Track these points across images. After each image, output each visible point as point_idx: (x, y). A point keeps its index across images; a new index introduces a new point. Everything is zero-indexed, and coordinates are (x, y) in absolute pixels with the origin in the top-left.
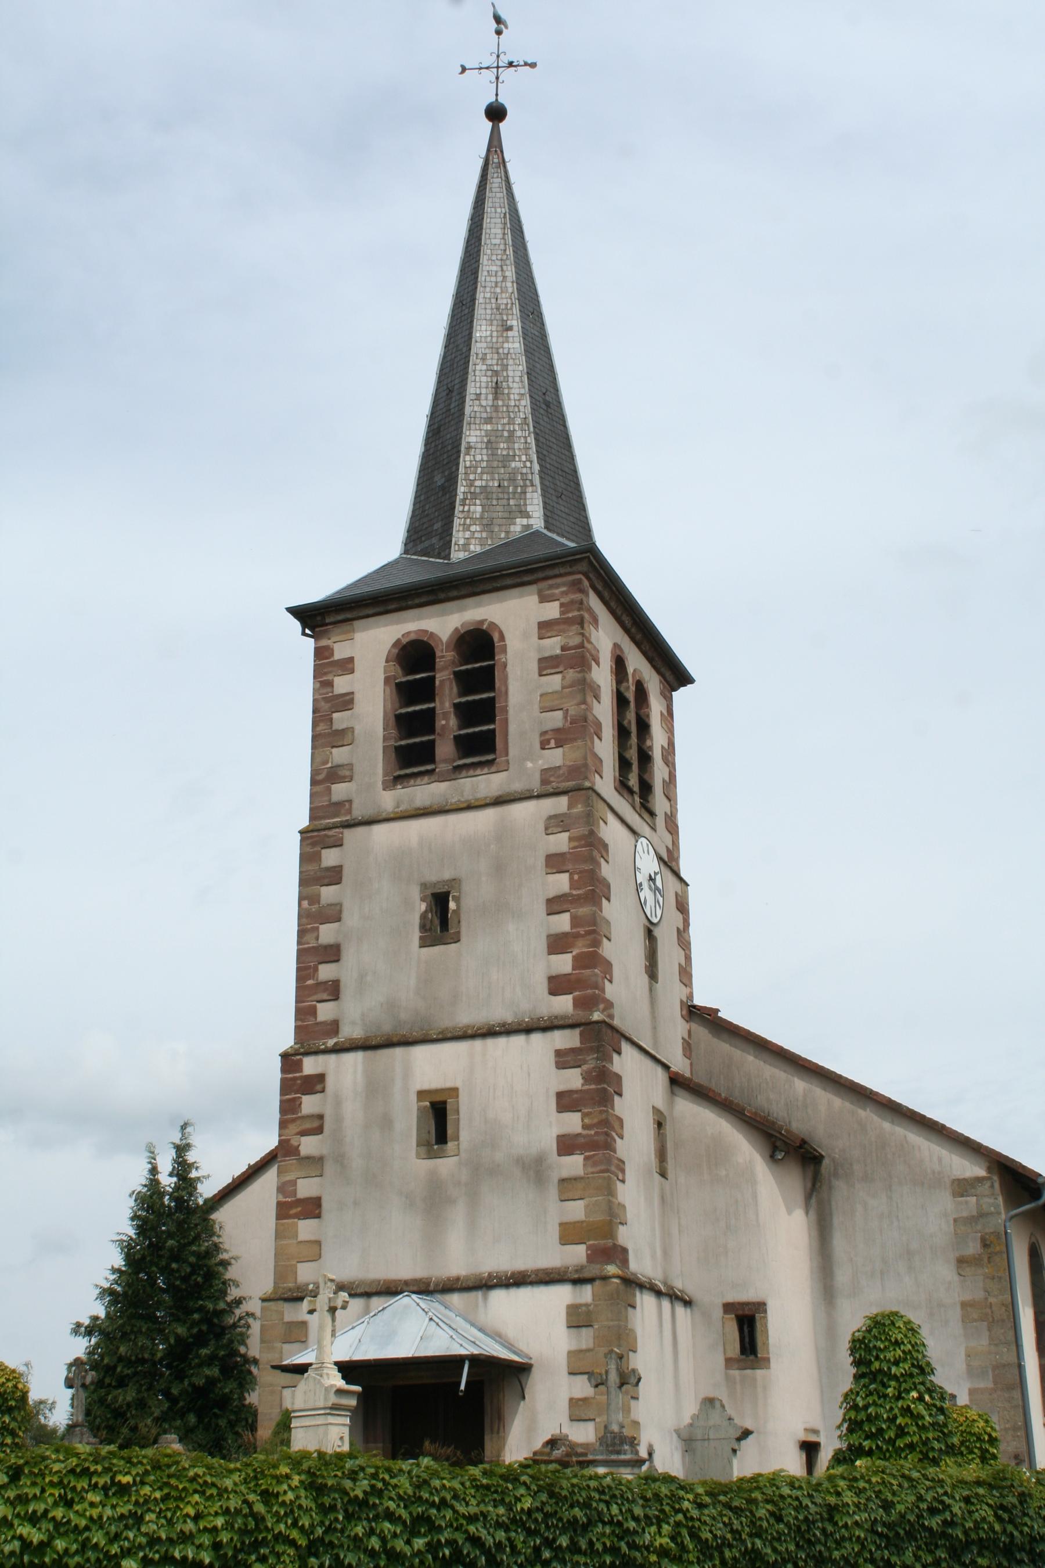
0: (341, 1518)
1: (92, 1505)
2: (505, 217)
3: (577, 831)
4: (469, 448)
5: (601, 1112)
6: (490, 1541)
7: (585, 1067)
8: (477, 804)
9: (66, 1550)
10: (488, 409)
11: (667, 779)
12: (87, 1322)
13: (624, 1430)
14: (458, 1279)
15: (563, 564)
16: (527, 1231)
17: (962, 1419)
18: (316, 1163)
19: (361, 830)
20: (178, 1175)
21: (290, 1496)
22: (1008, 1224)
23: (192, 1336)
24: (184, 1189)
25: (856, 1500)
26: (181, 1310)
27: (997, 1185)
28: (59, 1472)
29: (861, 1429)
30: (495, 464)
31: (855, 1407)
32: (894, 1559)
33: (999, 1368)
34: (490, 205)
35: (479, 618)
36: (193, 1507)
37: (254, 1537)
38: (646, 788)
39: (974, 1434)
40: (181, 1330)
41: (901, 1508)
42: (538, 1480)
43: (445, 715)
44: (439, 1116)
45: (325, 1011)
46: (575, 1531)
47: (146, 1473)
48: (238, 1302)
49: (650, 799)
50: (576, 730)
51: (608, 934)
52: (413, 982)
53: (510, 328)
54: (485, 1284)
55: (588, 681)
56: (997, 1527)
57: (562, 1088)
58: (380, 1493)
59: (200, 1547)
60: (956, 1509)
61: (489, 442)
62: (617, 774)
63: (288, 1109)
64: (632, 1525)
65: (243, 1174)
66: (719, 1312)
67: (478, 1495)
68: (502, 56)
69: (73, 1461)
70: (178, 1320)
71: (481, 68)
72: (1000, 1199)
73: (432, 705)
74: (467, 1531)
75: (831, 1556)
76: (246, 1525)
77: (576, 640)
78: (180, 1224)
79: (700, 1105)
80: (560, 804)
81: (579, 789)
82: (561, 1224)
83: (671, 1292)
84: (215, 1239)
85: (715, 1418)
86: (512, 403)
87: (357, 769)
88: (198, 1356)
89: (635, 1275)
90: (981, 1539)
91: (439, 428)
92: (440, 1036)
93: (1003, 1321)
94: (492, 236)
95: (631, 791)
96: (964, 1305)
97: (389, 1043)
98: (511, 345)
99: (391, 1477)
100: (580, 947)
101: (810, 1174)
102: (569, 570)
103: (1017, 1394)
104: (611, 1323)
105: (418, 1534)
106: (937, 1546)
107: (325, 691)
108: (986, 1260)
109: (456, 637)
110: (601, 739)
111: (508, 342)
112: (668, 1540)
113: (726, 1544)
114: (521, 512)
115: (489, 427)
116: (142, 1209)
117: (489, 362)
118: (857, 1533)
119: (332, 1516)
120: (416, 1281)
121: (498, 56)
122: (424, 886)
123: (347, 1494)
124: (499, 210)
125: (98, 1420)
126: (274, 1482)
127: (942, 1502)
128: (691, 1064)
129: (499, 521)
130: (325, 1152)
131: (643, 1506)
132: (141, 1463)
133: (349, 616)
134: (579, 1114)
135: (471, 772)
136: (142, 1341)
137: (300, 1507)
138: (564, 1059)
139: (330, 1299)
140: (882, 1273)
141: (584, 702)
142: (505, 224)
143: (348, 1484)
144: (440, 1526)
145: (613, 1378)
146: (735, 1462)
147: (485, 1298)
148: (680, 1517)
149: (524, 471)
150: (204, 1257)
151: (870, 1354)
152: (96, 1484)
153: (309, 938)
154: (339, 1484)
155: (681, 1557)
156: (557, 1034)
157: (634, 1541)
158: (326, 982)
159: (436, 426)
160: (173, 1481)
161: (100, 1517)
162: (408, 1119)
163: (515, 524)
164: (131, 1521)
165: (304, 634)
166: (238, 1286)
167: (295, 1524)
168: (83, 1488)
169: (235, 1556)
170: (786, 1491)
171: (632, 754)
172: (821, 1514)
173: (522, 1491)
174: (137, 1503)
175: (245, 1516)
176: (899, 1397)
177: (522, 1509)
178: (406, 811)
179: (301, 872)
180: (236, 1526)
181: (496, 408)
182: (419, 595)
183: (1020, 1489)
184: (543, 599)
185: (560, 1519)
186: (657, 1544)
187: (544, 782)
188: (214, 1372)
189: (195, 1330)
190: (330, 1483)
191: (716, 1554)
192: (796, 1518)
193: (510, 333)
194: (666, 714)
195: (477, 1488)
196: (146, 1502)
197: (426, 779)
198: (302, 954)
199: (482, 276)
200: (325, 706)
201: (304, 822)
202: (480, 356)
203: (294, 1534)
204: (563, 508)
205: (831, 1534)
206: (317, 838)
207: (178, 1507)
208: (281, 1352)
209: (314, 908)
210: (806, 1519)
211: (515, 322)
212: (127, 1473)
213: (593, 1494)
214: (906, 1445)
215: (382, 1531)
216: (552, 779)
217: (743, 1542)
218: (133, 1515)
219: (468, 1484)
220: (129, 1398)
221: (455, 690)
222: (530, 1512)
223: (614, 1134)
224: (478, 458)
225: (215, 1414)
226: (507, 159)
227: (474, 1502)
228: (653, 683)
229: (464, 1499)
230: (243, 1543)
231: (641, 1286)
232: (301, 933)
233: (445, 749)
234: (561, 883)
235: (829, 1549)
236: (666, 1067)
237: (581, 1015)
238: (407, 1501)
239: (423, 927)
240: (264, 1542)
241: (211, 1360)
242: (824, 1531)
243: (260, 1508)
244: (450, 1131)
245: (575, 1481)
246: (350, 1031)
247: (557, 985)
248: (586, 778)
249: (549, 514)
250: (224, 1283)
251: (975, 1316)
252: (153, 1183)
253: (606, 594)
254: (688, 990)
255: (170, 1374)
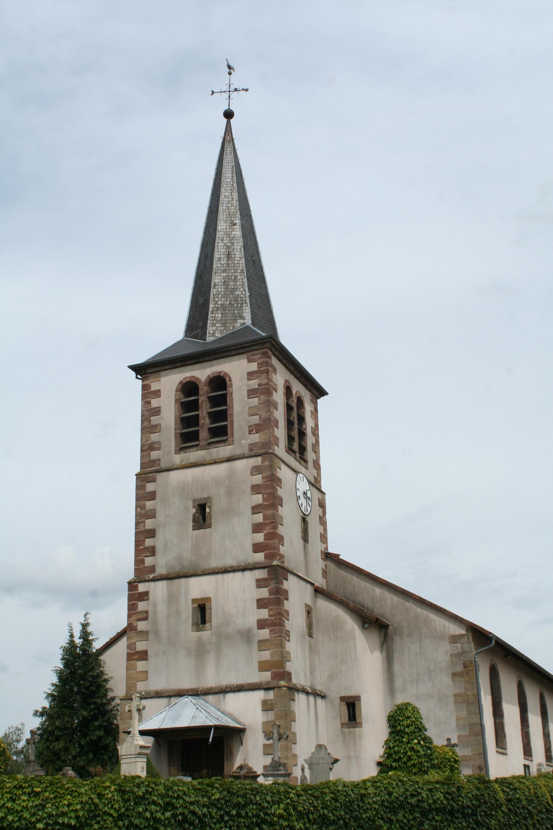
0: (132, 804)
1: (24, 801)
2: (233, 168)
3: (265, 474)
4: (215, 285)
5: (277, 608)
6: (200, 813)
7: (270, 587)
8: (219, 461)
9: (13, 820)
10: (225, 265)
11: (314, 443)
12: (40, 710)
13: (281, 760)
14: (211, 688)
15: (259, 344)
16: (243, 666)
17: (441, 752)
18: (145, 634)
19: (164, 474)
20: (83, 638)
21: (110, 795)
22: (476, 656)
23: (91, 716)
24: (86, 645)
25: (374, 791)
26: (86, 703)
27: (471, 638)
28: (10, 787)
29: (391, 757)
30: (228, 293)
31: (389, 748)
32: (393, 817)
33: (471, 726)
34: (226, 162)
35: (219, 370)
36: (67, 801)
37: (94, 813)
38: (303, 449)
39: (447, 758)
40: (85, 713)
41: (395, 794)
42: (223, 785)
43: (204, 418)
44: (202, 611)
45: (149, 561)
46: (239, 808)
47: (47, 787)
48: (113, 699)
49: (305, 454)
50: (267, 424)
51: (281, 522)
52: (190, 547)
53: (235, 224)
54: (224, 691)
55: (271, 400)
56: (445, 802)
57: (259, 597)
58: (150, 793)
59: (70, 818)
60: (424, 795)
61: (225, 282)
62: (287, 444)
63: (132, 608)
64: (266, 805)
65: (115, 637)
66: (338, 701)
67: (195, 793)
68: (231, 86)
69: (16, 782)
70: (83, 708)
71: (221, 92)
72: (472, 644)
73: (197, 413)
74: (189, 809)
75: (361, 817)
76: (90, 808)
77: (265, 381)
78: (84, 662)
79: (328, 602)
80: (258, 461)
81: (267, 453)
82: (259, 662)
83: (314, 692)
84: (101, 669)
85: (322, 753)
86: (236, 262)
87: (163, 444)
88: (94, 726)
89: (295, 685)
90: (437, 808)
91: (201, 274)
92: (202, 573)
93: (473, 703)
94: (227, 178)
95: (294, 452)
96: (455, 695)
97: (178, 577)
98: (235, 233)
99: (156, 786)
100: (268, 530)
101: (383, 634)
102: (261, 347)
103: (480, 738)
104: (282, 708)
105: (168, 811)
106: (415, 811)
107: (147, 406)
108: (465, 674)
109: (208, 380)
110: (278, 428)
111: (234, 231)
112: (283, 811)
113: (309, 812)
114: (240, 316)
115: (225, 274)
116: (67, 655)
117: (225, 242)
118: (375, 806)
119: (128, 804)
120: (192, 690)
121: (230, 86)
122: (194, 501)
123: (135, 794)
124: (230, 164)
125: (46, 757)
126: (103, 789)
127: (417, 791)
128: (327, 581)
129: (229, 321)
130: (149, 628)
131: (271, 796)
132: (45, 782)
133: (158, 369)
134: (267, 610)
135: (216, 446)
136: (66, 719)
137: (114, 800)
138: (260, 584)
139: (137, 705)
140: (417, 681)
141: (269, 411)
142: (233, 171)
143: (136, 789)
144: (177, 807)
145: (276, 736)
146: (331, 774)
147: (224, 698)
148: (289, 801)
149: (242, 296)
150: (96, 678)
151: (396, 722)
152: (25, 792)
153: (141, 526)
154: (131, 790)
155: (288, 818)
156: (257, 571)
157: (266, 812)
158: (149, 547)
159: (200, 273)
160: (58, 790)
161: (27, 806)
162: (187, 613)
163: (237, 323)
164: (40, 807)
165: (137, 378)
166: (112, 691)
167: (112, 807)
168: (20, 794)
169: (86, 821)
170: (340, 788)
171: (295, 433)
172: (357, 798)
173: (215, 791)
174: (43, 799)
175: (90, 804)
176: (409, 743)
177: (215, 799)
178: (186, 464)
179: (136, 494)
180: (86, 808)
181: (228, 265)
182: (191, 359)
183: (458, 784)
184: (250, 361)
185: (232, 803)
186: (277, 813)
187: (250, 450)
188: (101, 733)
189: (92, 713)
190: (127, 789)
191: (305, 817)
192: (345, 800)
193: (235, 227)
194: (314, 411)
195: (195, 790)
196: (47, 799)
197: (195, 449)
198: (137, 534)
199: (222, 198)
200: (147, 413)
201: (138, 470)
202: (221, 239)
203: (112, 811)
204: (261, 313)
205: (362, 807)
206: (143, 478)
207: (60, 801)
208: (130, 724)
209: (143, 511)
210: (350, 800)
211: (238, 221)
212: (39, 787)
213: (247, 791)
214: (411, 765)
215: (151, 809)
216: (254, 449)
217: (319, 811)
218: (41, 805)
219: (191, 788)
220: (60, 747)
221: (208, 405)
222: (218, 799)
223: (284, 619)
224: (220, 290)
225: (102, 753)
226: (234, 138)
227: (193, 796)
228: (306, 396)
229: (189, 795)
230: (89, 816)
231: (298, 690)
232: (137, 524)
233: (204, 434)
234: (258, 499)
235: (361, 814)
236: (312, 584)
237: (268, 563)
238: (162, 796)
239: (194, 521)
240: (99, 815)
241: (99, 728)
242: (358, 805)
243: (96, 801)
244: (207, 619)
245: (239, 786)
246: (161, 570)
247: (257, 548)
248: (270, 448)
249: (254, 317)
250: (106, 690)
251: (460, 701)
252: (72, 642)
253: (281, 357)
254: (325, 545)
255: (80, 735)
